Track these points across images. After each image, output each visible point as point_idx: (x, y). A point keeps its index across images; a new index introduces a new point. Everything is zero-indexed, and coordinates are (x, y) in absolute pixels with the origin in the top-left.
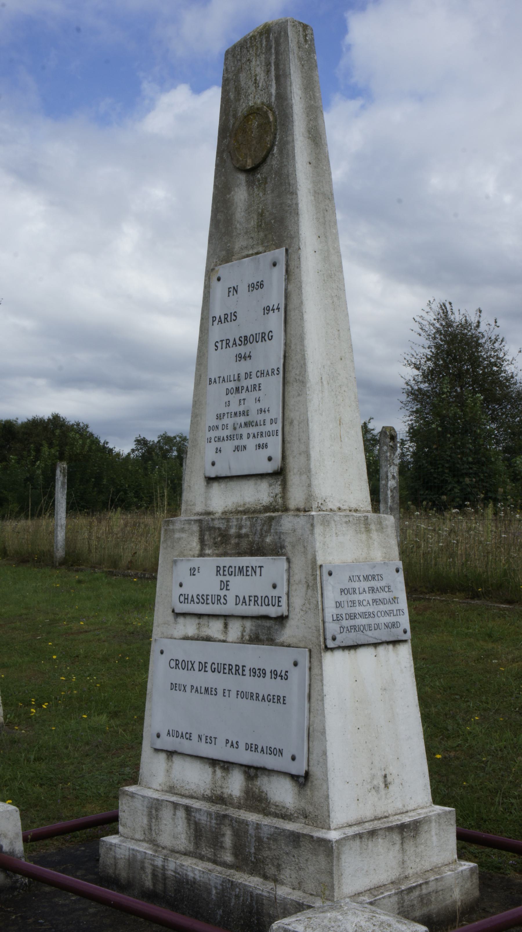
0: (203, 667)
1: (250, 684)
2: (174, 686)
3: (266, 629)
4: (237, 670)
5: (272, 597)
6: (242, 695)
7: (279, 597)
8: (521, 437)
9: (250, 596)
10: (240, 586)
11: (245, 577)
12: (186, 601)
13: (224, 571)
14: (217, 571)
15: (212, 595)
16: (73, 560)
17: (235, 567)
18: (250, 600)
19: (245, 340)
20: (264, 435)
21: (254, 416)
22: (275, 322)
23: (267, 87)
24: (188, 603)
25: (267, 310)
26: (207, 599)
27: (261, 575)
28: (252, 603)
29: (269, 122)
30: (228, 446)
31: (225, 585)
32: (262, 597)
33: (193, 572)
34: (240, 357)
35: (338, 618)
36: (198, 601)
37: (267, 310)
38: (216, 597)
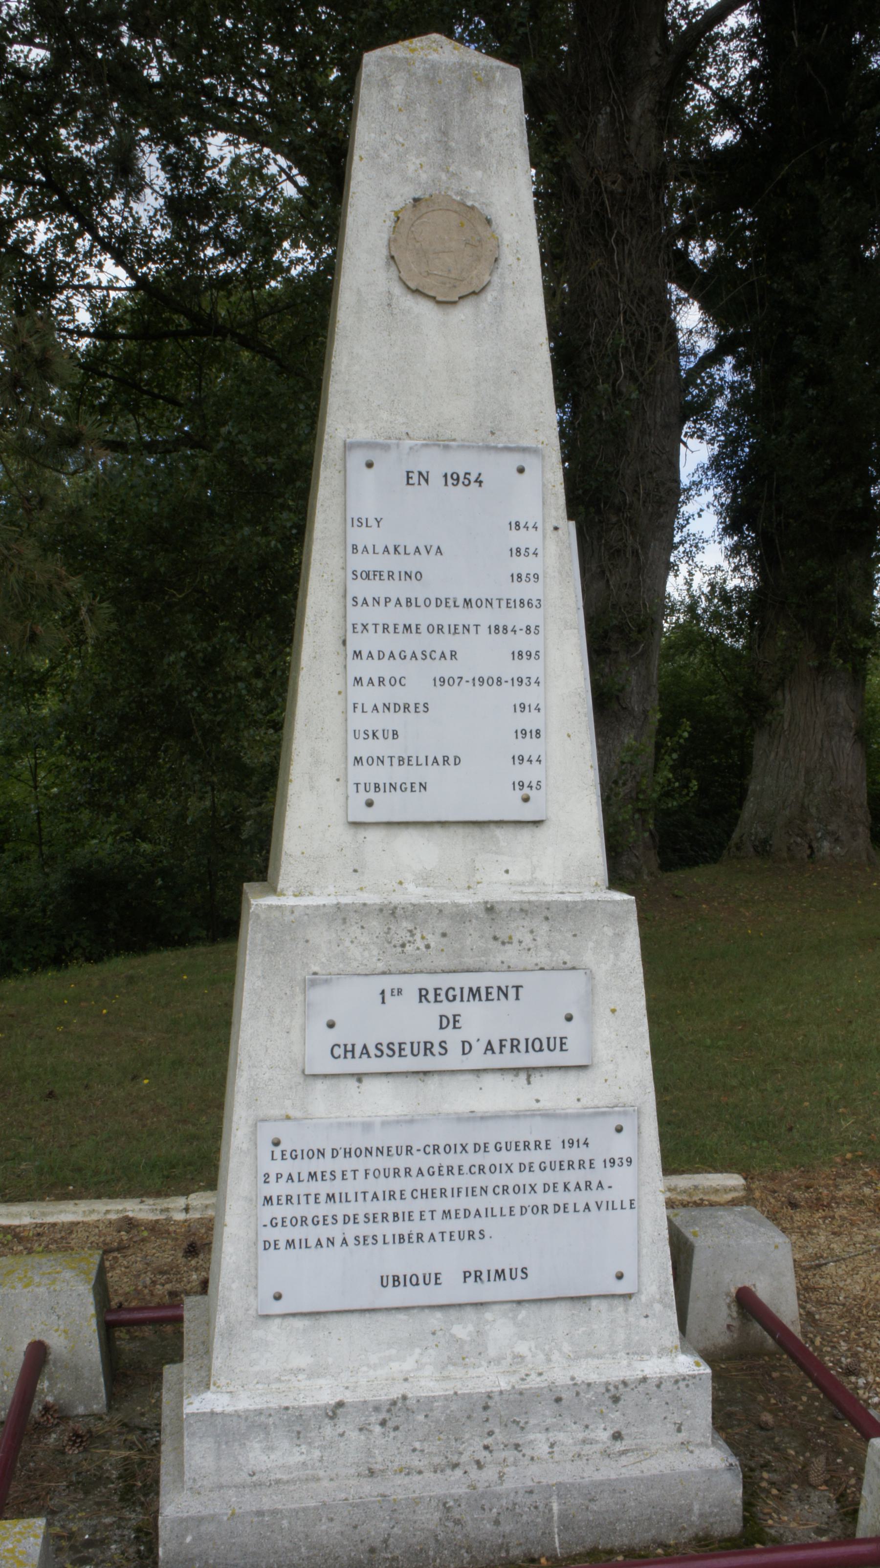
5: (548, 1039)
7: (561, 1039)
8: (878, 777)
9: (501, 1041)
11: (484, 1002)
12: (349, 1055)
13: (436, 995)
14: (421, 996)
15: (412, 1043)
17: (462, 989)
18: (502, 1046)
20: (522, 1047)
24: (353, 1057)
26: (401, 1049)
27: (517, 998)
29: (559, 1497)
32: (527, 1040)
36: (379, 1053)
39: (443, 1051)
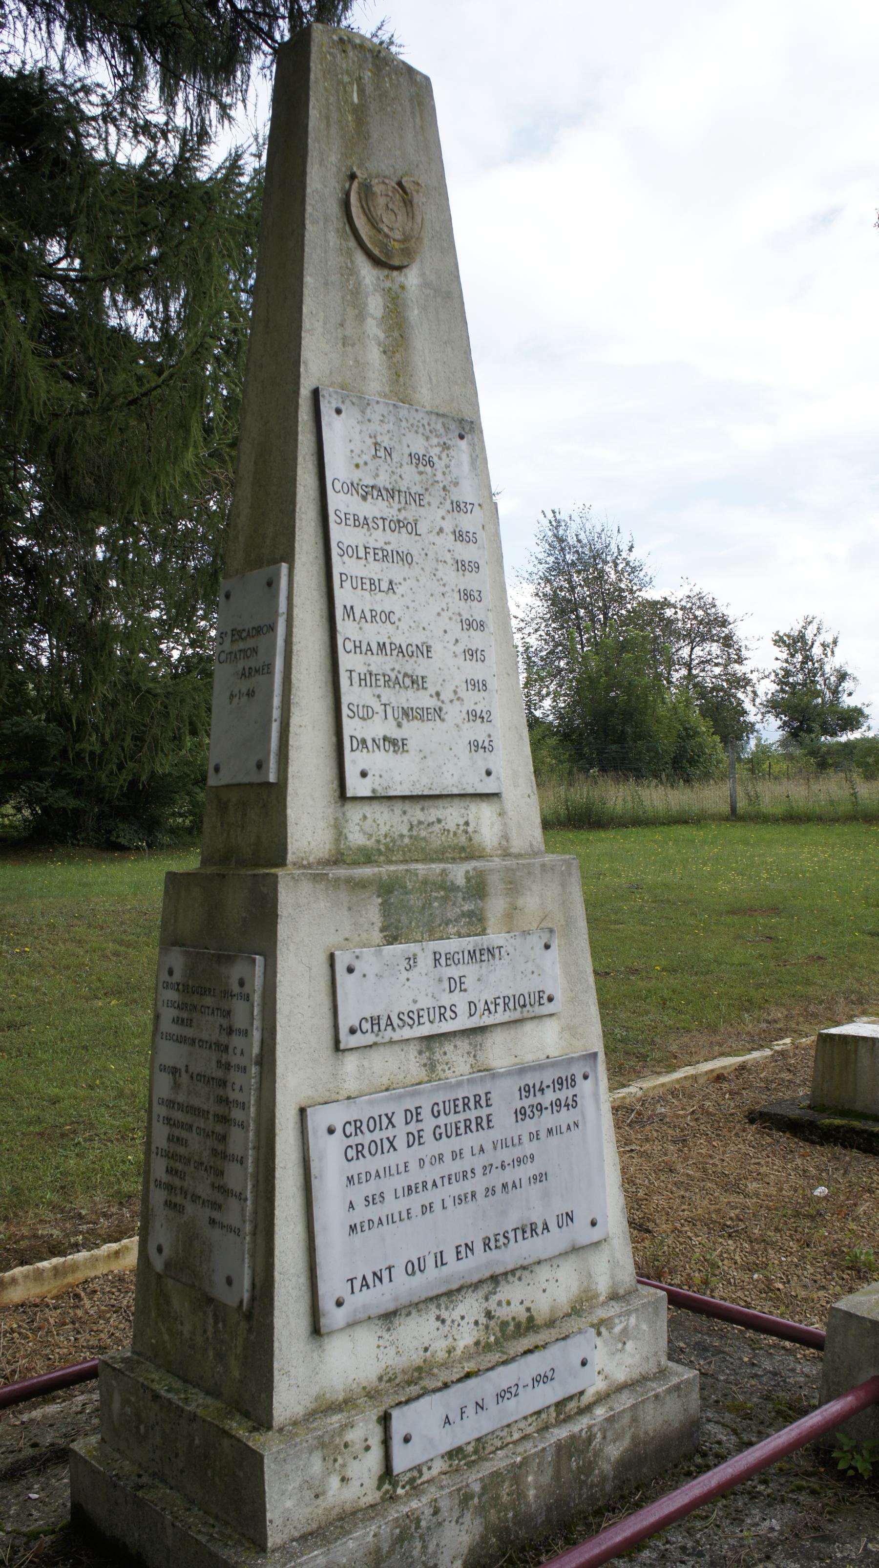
12: (358, 650)
28: (500, 1009)
38: (437, 1010)
39: (453, 1015)
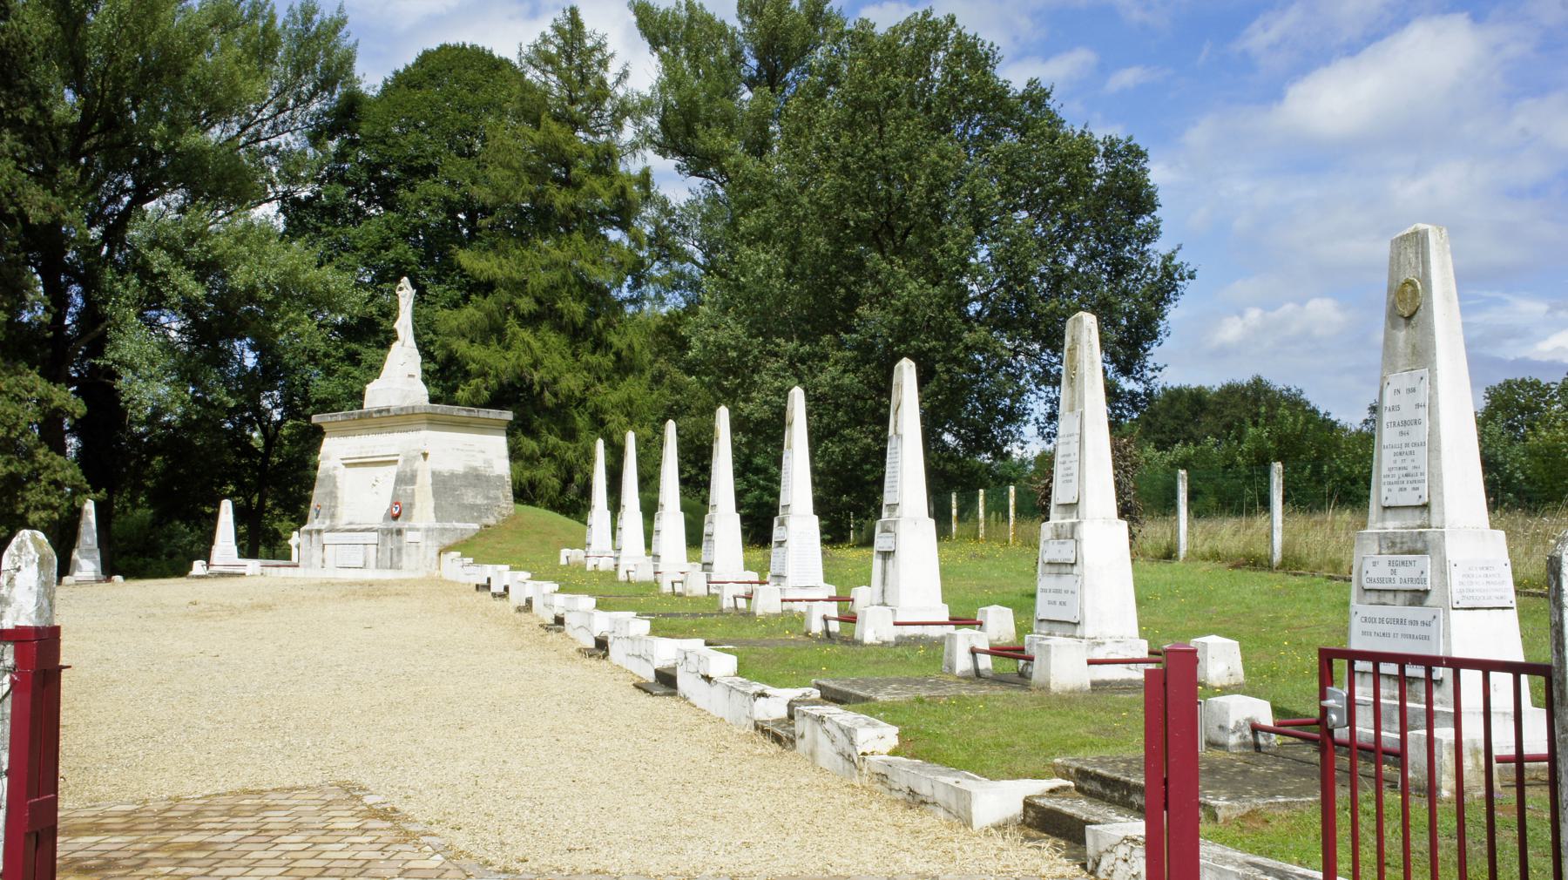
0: (1382, 620)
1: (1410, 630)
2: (1364, 633)
3: (1418, 597)
4: (1402, 622)
6: (1405, 636)
10: (1403, 572)
16: (1292, 564)
19: (1405, 423)
21: (1410, 470)
22: (1423, 414)
23: (1416, 268)
25: (1418, 406)
30: (1396, 488)
31: (1394, 572)
33: (1374, 564)
34: (1402, 433)
35: (1461, 591)
37: (1418, 406)
